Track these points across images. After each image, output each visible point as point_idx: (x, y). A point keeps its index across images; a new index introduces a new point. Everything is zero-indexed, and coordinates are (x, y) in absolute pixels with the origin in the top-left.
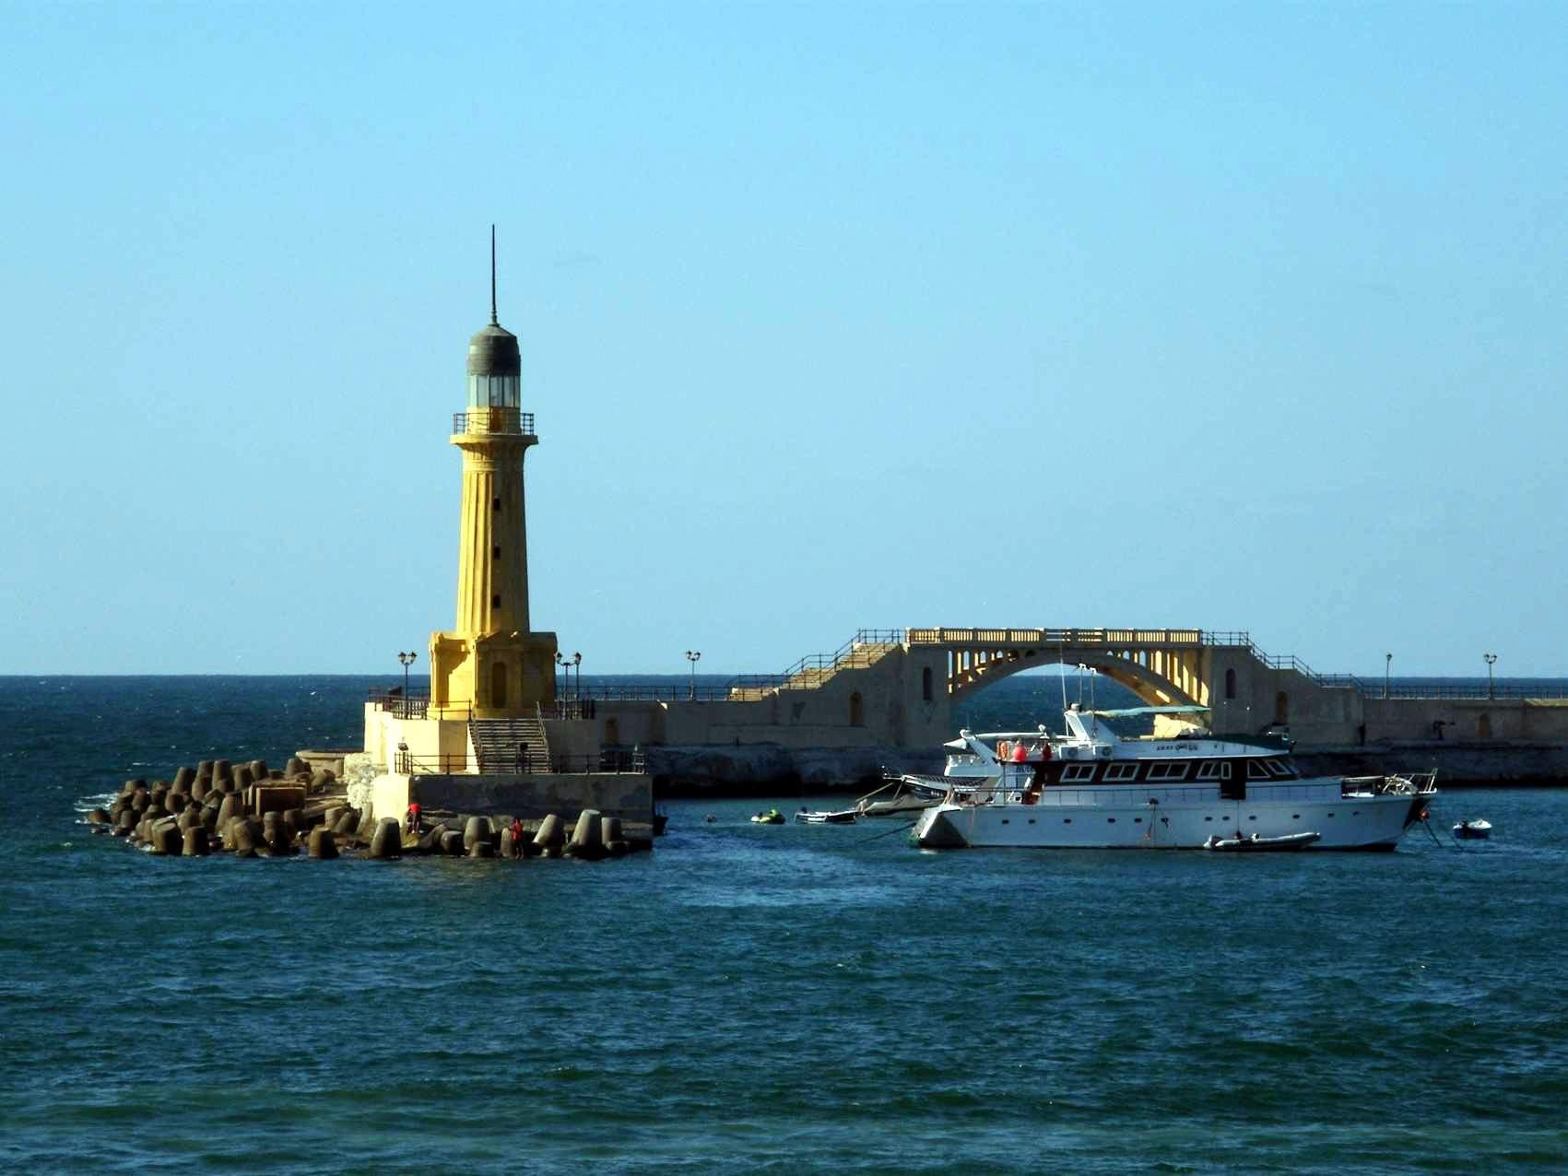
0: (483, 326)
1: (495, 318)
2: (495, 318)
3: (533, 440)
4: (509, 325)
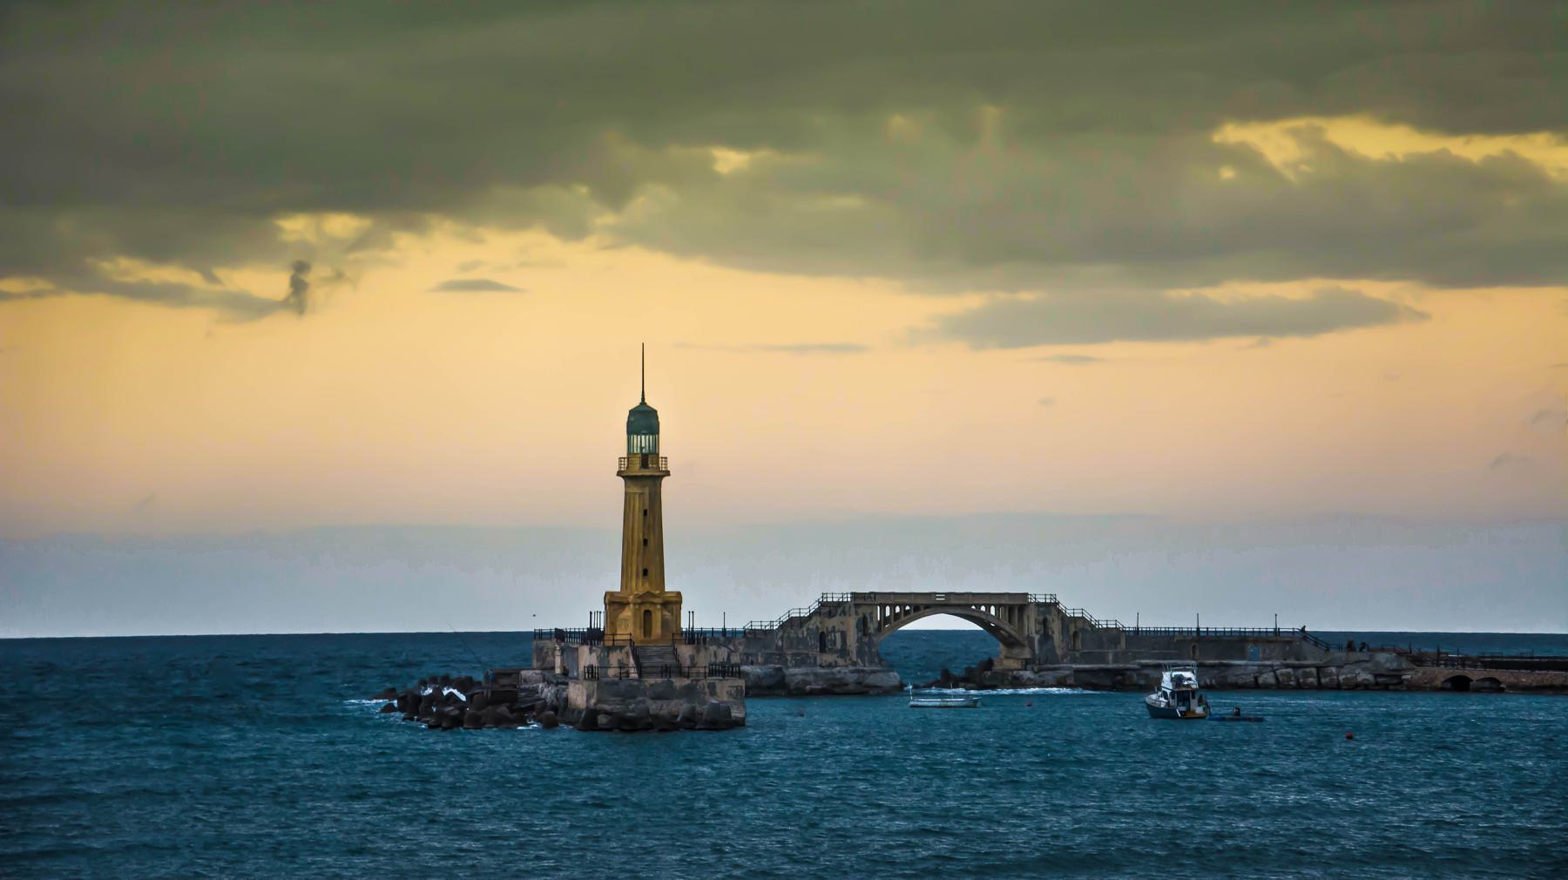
3: (668, 473)
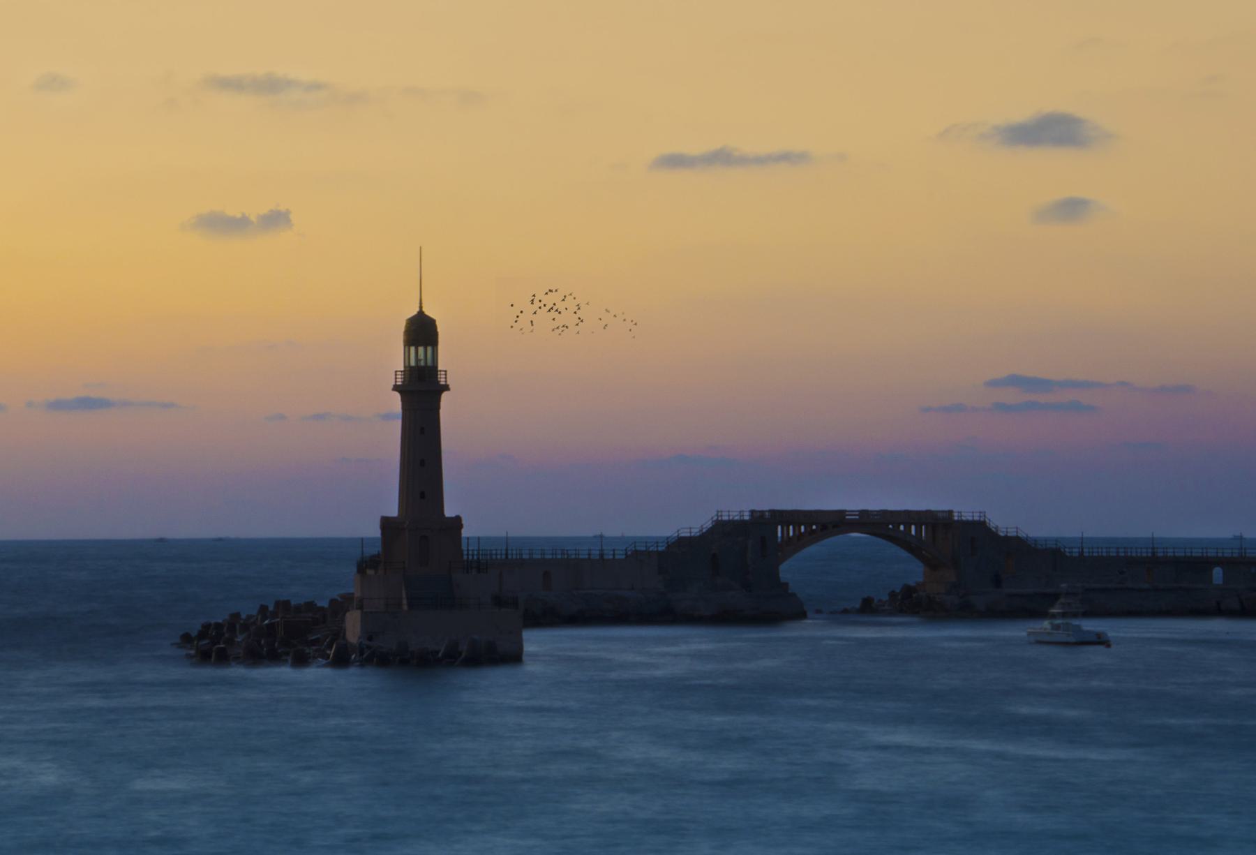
0: (415, 311)
1: (421, 307)
2: (421, 307)
3: (446, 388)
4: (427, 312)
